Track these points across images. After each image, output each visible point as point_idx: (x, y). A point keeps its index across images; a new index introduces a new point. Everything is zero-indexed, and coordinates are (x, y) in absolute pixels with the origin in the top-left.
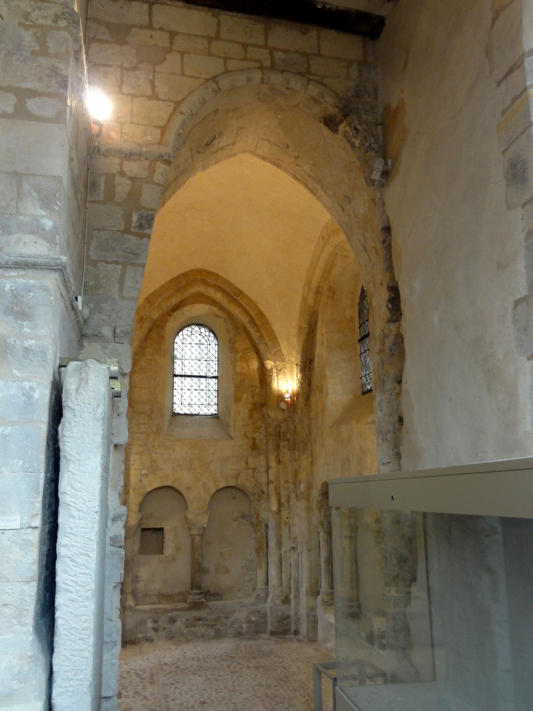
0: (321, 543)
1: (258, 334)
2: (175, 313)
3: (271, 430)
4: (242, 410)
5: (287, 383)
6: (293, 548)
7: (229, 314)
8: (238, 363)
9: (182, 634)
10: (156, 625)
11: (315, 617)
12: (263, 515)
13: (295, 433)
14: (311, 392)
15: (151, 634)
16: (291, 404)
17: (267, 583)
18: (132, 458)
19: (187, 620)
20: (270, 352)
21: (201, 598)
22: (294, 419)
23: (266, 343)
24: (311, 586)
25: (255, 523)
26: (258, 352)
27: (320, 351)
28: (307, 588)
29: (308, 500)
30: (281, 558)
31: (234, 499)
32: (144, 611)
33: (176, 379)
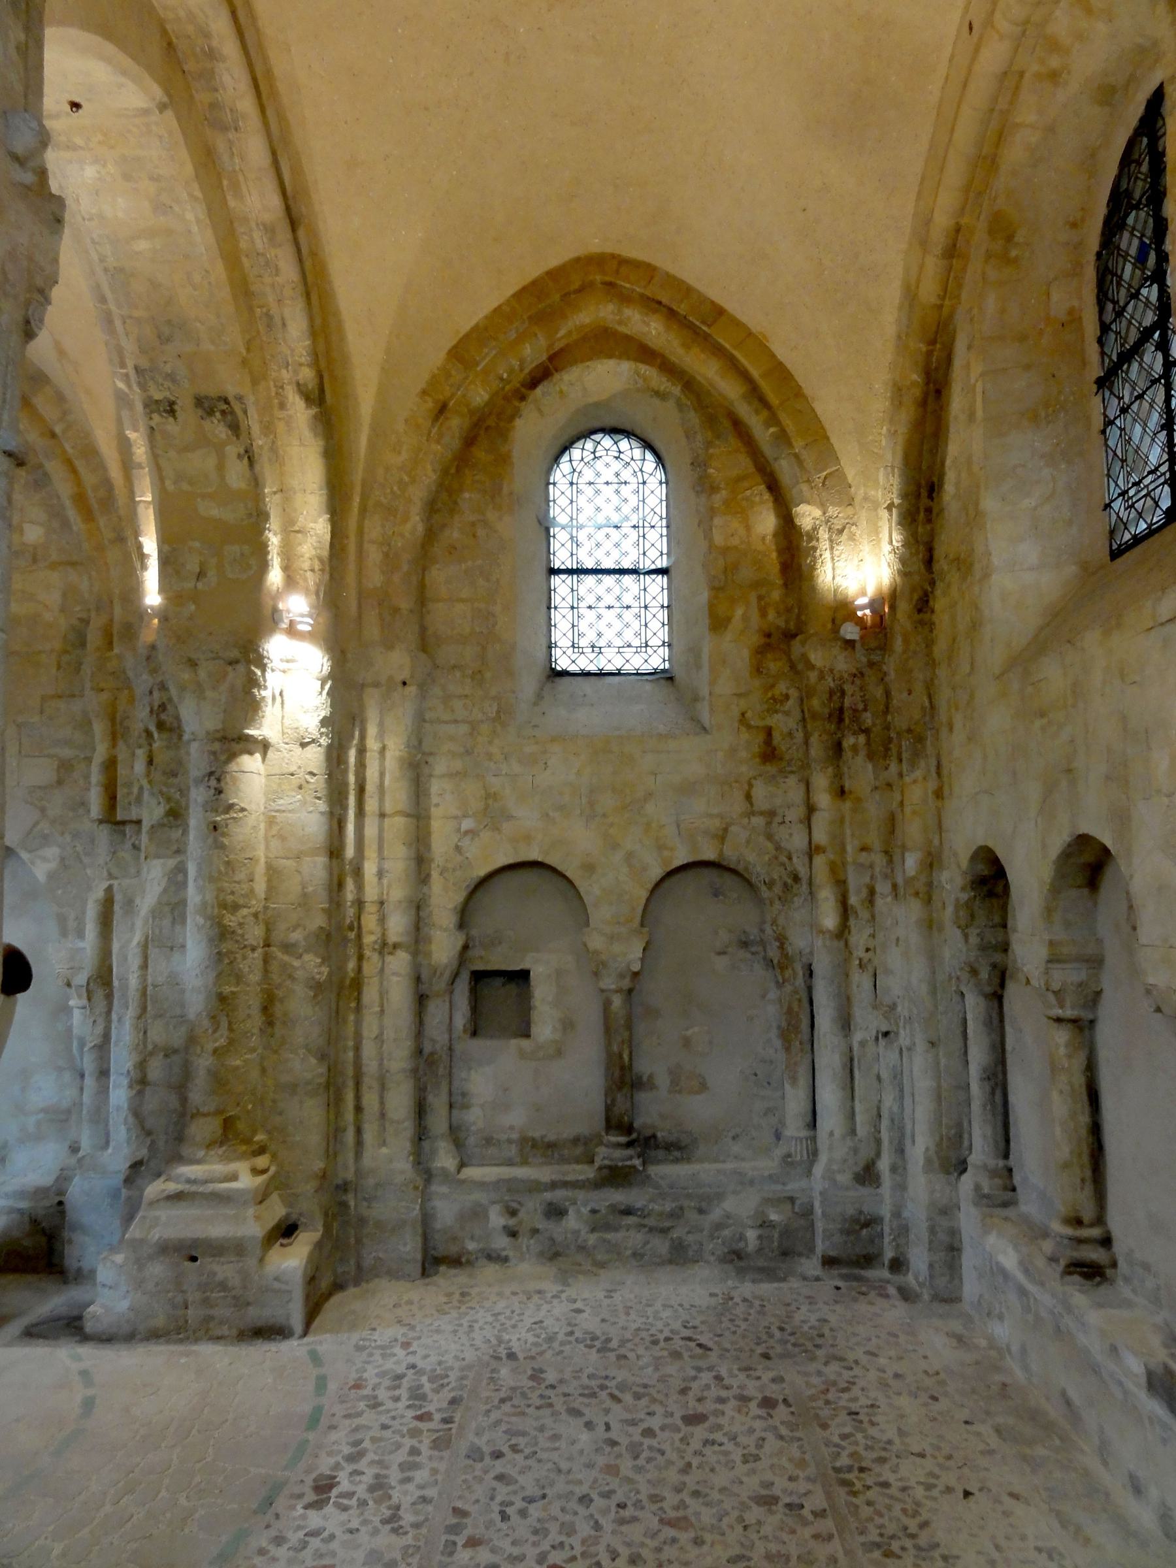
0: (970, 1023)
1: (772, 430)
2: (539, 391)
3: (815, 703)
4: (737, 648)
5: (860, 566)
6: (886, 1034)
7: (689, 384)
8: (717, 521)
9: (582, 1248)
10: (512, 1222)
11: (954, 1233)
12: (799, 941)
13: (887, 710)
14: (933, 583)
15: (501, 1242)
16: (873, 626)
17: (813, 1124)
18: (435, 787)
19: (594, 1211)
20: (808, 481)
21: (631, 1158)
22: (885, 668)
23: (796, 456)
24: (939, 1145)
25: (775, 962)
26: (774, 487)
27: (964, 442)
28: (927, 1149)
29: (929, 901)
30: (852, 1060)
31: (716, 895)
32: (482, 1185)
33: (556, 581)
